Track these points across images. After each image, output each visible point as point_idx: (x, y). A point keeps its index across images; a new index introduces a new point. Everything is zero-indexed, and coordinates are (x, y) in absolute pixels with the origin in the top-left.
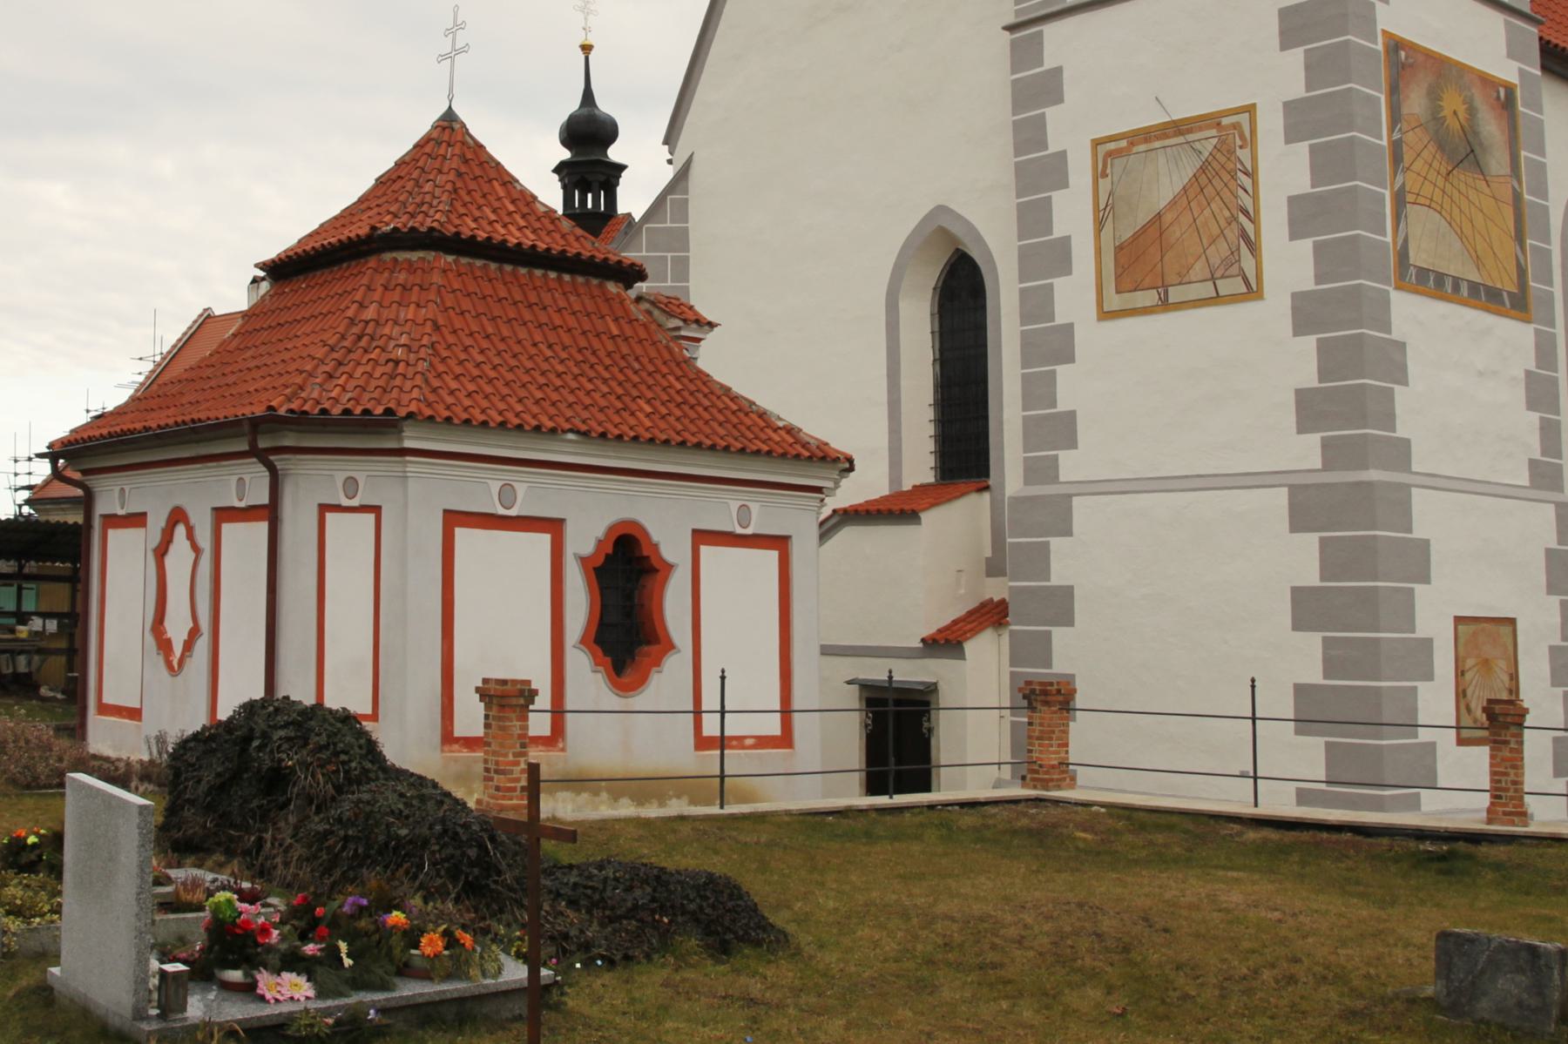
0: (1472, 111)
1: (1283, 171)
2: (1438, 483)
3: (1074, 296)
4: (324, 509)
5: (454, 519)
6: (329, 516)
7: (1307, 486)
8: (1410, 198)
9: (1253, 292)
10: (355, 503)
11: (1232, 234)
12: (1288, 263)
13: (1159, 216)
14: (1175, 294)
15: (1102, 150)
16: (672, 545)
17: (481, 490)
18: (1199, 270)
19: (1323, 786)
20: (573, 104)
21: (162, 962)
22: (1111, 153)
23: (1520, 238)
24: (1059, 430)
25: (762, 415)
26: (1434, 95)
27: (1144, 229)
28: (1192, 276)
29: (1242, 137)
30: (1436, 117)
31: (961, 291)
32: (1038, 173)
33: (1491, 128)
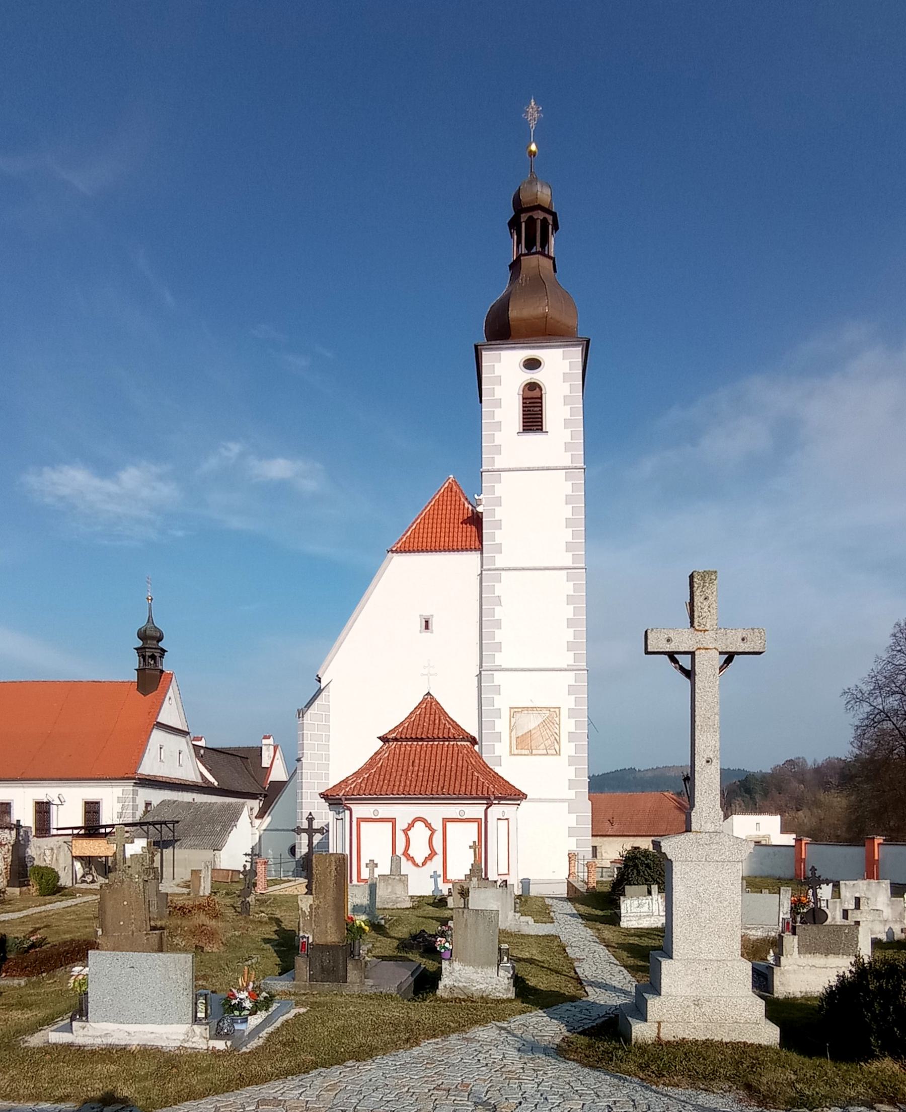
1: (568, 725)
7: (207, 768)
9: (558, 753)
11: (552, 739)
12: (568, 748)
14: (534, 752)
15: (513, 711)
18: (542, 746)
21: (526, 222)
22: (515, 711)
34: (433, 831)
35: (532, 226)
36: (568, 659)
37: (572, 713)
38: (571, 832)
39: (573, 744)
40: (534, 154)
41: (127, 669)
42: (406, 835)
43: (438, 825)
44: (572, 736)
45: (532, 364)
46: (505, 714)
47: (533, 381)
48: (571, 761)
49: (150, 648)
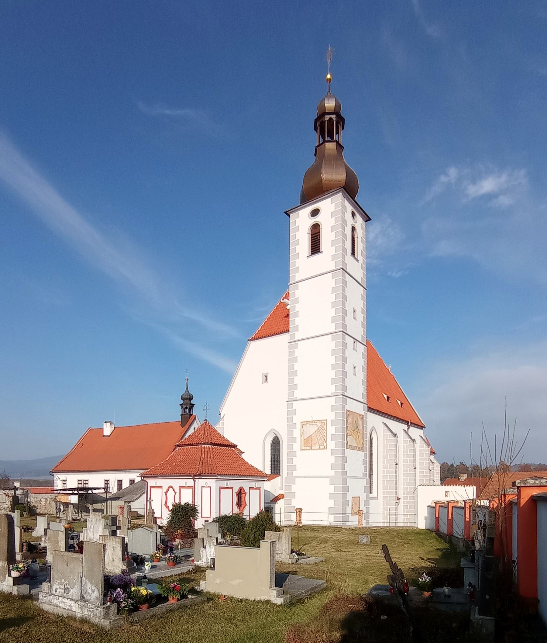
1: (331, 430)
2: (351, 477)
3: (297, 446)
5: (221, 488)
9: (325, 448)
11: (323, 439)
12: (331, 445)
14: (313, 448)
16: (247, 491)
17: (224, 483)
18: (317, 444)
22: (304, 424)
25: (257, 469)
31: (276, 444)
32: (291, 426)
33: (360, 422)
35: (328, 126)
36: (331, 389)
40: (330, 79)
41: (176, 415)
42: (166, 495)
43: (177, 490)
44: (333, 437)
45: (315, 212)
46: (299, 426)
48: (333, 452)
49: (188, 404)
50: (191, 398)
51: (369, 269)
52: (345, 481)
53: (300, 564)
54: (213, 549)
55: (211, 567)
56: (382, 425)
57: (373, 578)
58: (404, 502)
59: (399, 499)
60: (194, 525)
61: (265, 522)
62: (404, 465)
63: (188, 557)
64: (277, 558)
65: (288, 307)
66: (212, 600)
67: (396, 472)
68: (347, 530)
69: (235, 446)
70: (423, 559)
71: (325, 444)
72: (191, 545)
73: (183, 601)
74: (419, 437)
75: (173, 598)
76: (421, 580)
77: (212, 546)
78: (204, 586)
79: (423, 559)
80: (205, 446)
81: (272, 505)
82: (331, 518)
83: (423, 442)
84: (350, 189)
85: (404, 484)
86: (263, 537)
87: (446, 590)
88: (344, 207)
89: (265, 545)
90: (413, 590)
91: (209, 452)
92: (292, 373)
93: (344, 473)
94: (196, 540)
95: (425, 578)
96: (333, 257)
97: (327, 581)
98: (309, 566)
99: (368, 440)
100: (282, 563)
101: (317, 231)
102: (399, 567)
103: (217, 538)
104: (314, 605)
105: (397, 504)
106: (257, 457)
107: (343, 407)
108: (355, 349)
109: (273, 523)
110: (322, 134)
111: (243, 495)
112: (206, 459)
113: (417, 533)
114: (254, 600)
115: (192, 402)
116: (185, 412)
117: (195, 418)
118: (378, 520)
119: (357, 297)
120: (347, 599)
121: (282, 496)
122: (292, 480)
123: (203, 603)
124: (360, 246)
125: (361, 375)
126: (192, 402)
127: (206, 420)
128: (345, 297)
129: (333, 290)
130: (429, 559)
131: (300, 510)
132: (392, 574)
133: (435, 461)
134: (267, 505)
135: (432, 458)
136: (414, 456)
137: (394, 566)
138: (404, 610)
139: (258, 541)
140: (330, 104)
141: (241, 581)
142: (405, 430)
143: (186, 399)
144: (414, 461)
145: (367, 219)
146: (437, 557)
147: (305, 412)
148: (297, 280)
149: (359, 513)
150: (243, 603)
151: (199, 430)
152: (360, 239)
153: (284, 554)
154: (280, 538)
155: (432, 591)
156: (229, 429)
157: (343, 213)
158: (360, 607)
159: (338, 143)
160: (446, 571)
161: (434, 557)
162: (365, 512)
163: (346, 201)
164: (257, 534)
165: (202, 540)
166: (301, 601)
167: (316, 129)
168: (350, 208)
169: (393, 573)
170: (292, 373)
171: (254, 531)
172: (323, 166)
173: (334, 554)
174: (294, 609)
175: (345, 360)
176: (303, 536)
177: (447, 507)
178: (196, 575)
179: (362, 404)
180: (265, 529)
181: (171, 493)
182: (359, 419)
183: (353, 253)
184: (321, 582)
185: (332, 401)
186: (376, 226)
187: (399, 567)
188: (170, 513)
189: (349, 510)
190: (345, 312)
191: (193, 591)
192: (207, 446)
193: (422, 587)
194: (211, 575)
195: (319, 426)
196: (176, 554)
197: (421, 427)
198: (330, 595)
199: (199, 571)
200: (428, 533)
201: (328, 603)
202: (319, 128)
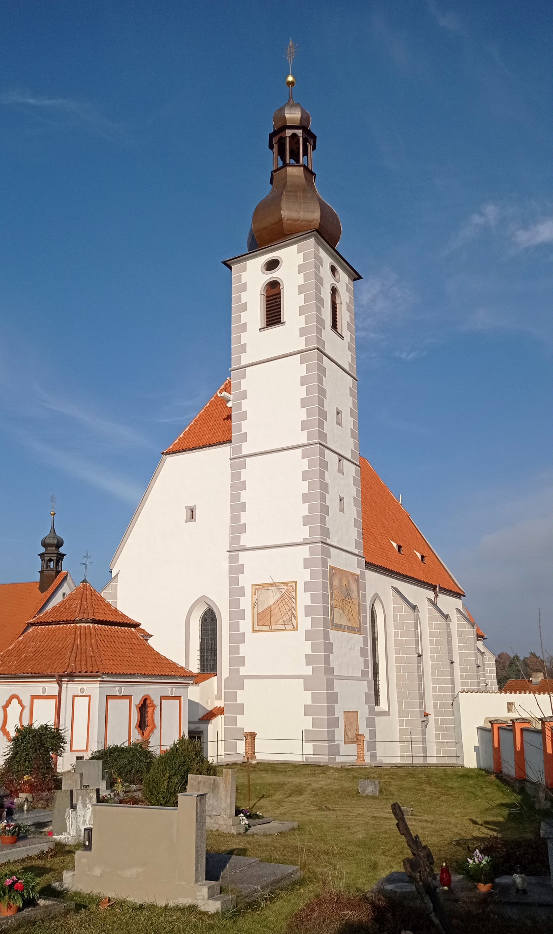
0: (349, 583)
1: (304, 599)
3: (245, 626)
4: (74, 696)
6: (75, 698)
8: (334, 606)
9: (295, 628)
10: (83, 694)
11: (290, 613)
13: (270, 607)
14: (274, 627)
16: (157, 702)
17: (115, 690)
18: (281, 622)
19: (312, 756)
20: (47, 533)
22: (257, 588)
23: (359, 614)
24: (238, 661)
25: (175, 664)
26: (340, 580)
27: (266, 610)
28: (279, 623)
29: (293, 589)
30: (341, 586)
31: (209, 621)
32: (236, 592)
33: (354, 587)
34: (23, 707)
35: (290, 144)
36: (304, 533)
37: (308, 587)
38: (308, 710)
39: (309, 618)
40: (292, 83)
41: (32, 571)
43: (26, 702)
44: (308, 611)
45: (272, 265)
46: (248, 592)
47: (272, 280)
48: (308, 635)
49: (53, 553)
50: (59, 544)
51: (360, 347)
52: (330, 685)
53: (253, 835)
54: (90, 811)
55: (85, 845)
56: (391, 591)
57: (388, 859)
58: (436, 721)
59: (426, 715)
60: (56, 765)
61: (190, 757)
62: (432, 658)
63: (40, 825)
64: (210, 823)
65: (229, 405)
66: (85, 907)
67: (420, 668)
68: (337, 770)
69: (136, 625)
70: (475, 823)
71: (294, 621)
72: (48, 802)
73: (28, 912)
74: (455, 611)
75: (9, 907)
76: (471, 862)
77: (89, 805)
78: (70, 881)
79: (475, 823)
80: (83, 625)
81: (202, 726)
82: (309, 748)
83: (462, 619)
84: (327, 234)
85: (434, 689)
86: (183, 786)
87: (518, 879)
88: (319, 260)
89: (186, 801)
90: (459, 881)
91: (88, 635)
92: (237, 507)
93: (329, 670)
94: (58, 794)
95: (479, 859)
96: (303, 332)
97: (303, 866)
98: (269, 839)
99: (368, 615)
100: (219, 834)
101: (275, 291)
102: (424, 844)
103: (98, 791)
104: (279, 911)
105: (425, 723)
106: (175, 642)
107: (324, 563)
108: (340, 471)
109: (203, 760)
110: (282, 153)
111: (149, 710)
112: (84, 647)
113: (462, 776)
114: (166, 906)
115: (62, 550)
116: (48, 566)
117: (65, 578)
118: (392, 751)
119: (341, 392)
120: (340, 902)
121: (221, 711)
122: (236, 682)
123: (67, 912)
124: (344, 316)
125: (353, 511)
126: (62, 550)
127: (85, 581)
128: (322, 392)
129: (304, 381)
130: (486, 823)
131: (253, 735)
132: (411, 856)
133: (486, 651)
134: (193, 727)
135: (480, 644)
136: (450, 642)
137: (414, 842)
138: (437, 921)
139: (174, 793)
140: (293, 115)
141: (140, 870)
142: (430, 600)
143: (51, 545)
144: (450, 650)
145: (356, 277)
146: (501, 819)
147: (258, 569)
148: (243, 363)
149: (358, 739)
150: (145, 912)
151: (72, 597)
152: (344, 307)
153: (222, 816)
154: (215, 787)
155: (492, 881)
156: (128, 598)
157: (317, 268)
158: (361, 915)
159: (306, 168)
160: (518, 844)
161: (495, 819)
162: (367, 738)
163: (321, 250)
164: (175, 780)
165: (69, 793)
166: (252, 905)
167: (271, 147)
168: (327, 260)
169: (414, 854)
170: (237, 507)
171: (167, 775)
172: (284, 198)
173: (316, 816)
174: (240, 920)
175: (324, 487)
176: (258, 781)
177: (511, 729)
178: (57, 860)
179: (356, 558)
180: (188, 771)
181: (14, 709)
182: (351, 582)
183: (334, 326)
184: (291, 868)
185: (305, 552)
186: (370, 286)
187: (424, 844)
188: (9, 744)
189: (340, 734)
190: (323, 414)
191: (49, 892)
192: (86, 625)
193: (475, 876)
194: (84, 861)
195: (284, 590)
196: (19, 822)
197: (458, 595)
198: (308, 893)
199: (62, 851)
200: (482, 775)
201: (303, 910)
202: (276, 146)
